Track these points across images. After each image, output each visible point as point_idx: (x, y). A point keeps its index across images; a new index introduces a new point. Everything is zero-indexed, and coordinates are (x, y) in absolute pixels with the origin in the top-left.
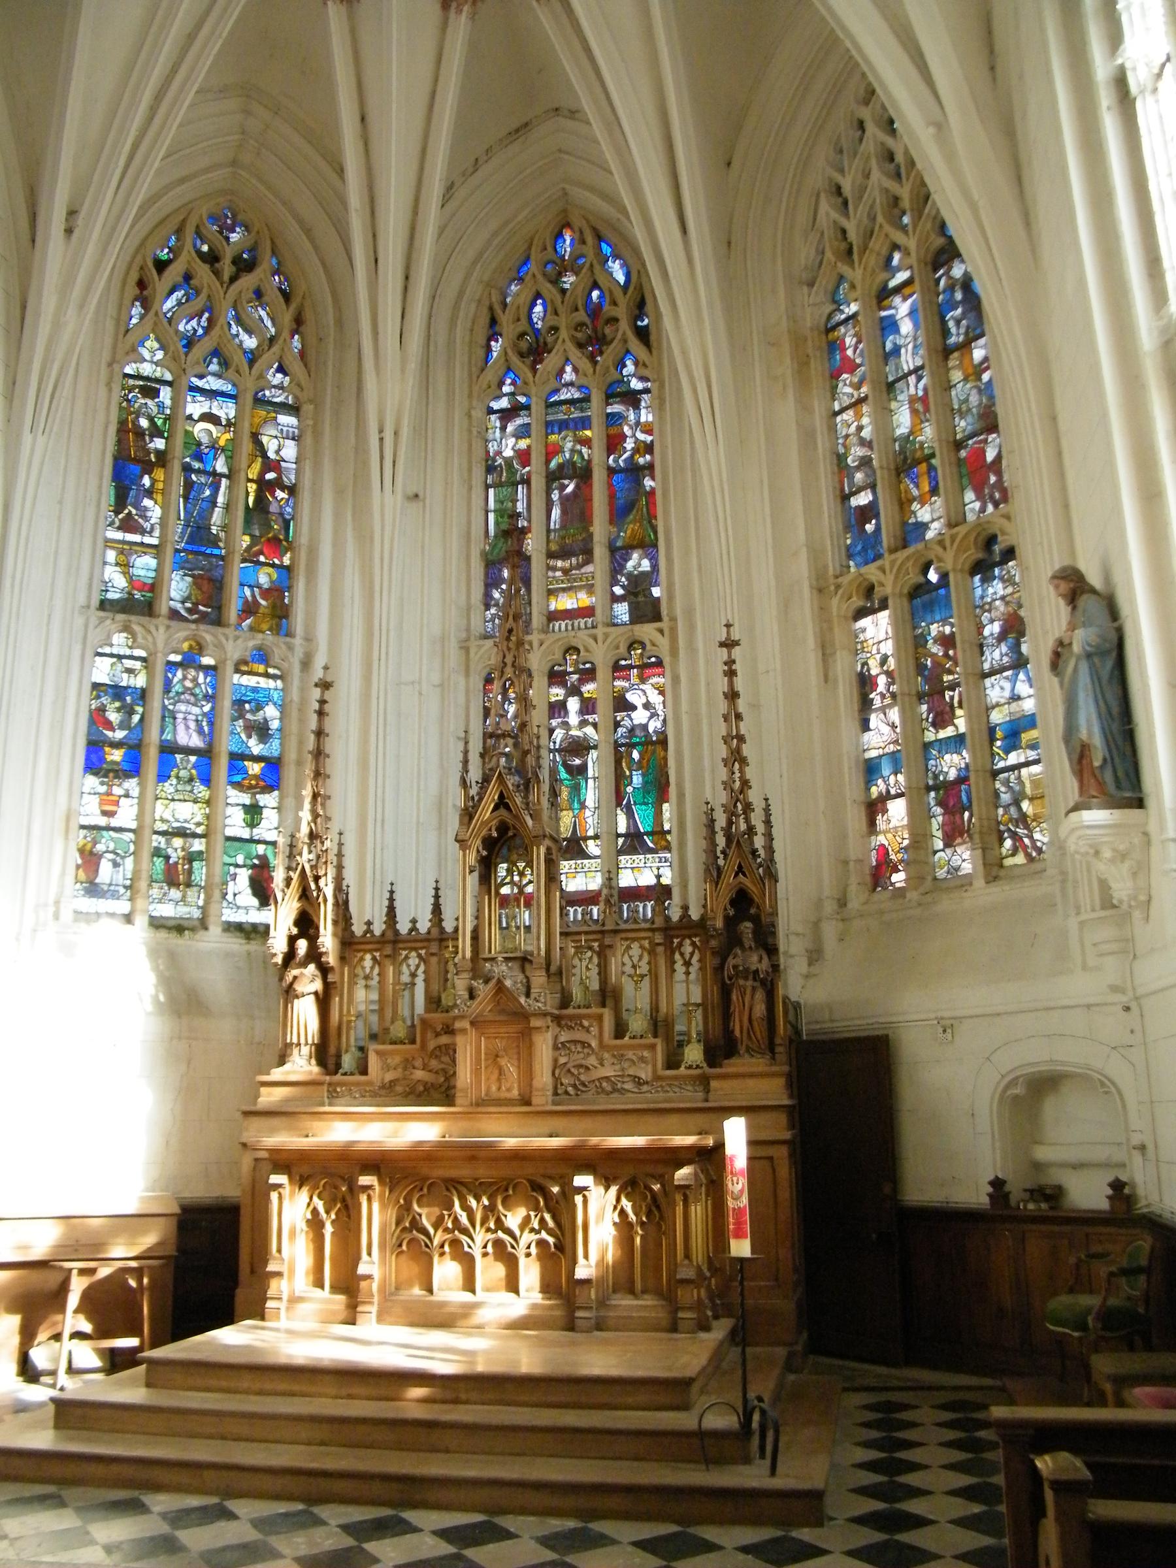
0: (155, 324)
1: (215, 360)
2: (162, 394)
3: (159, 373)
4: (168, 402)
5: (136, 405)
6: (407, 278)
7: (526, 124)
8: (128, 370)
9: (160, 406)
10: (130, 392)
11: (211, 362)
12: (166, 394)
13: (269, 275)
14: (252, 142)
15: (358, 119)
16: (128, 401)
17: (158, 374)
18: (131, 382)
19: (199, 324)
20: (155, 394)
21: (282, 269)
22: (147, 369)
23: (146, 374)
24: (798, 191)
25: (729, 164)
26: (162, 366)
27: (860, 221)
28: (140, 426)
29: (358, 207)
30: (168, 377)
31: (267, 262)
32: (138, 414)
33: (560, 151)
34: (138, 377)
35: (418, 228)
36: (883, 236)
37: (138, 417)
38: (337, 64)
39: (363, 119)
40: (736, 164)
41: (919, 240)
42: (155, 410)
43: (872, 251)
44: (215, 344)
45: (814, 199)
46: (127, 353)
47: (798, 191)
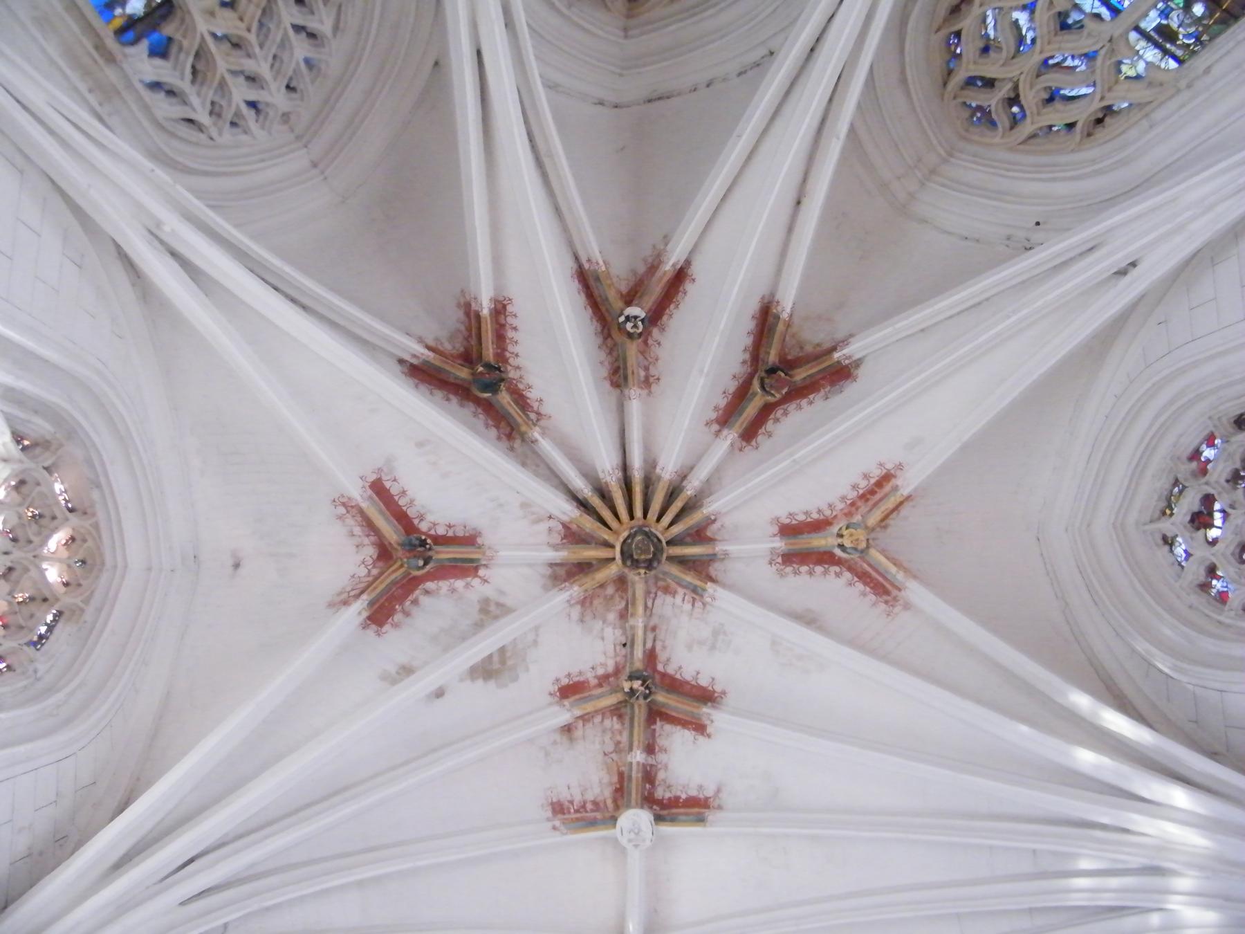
0: (1110, 89)
1: (1070, 21)
2: (1154, 25)
3: (1141, 44)
4: (1153, 14)
5: (1192, 30)
6: (812, 50)
7: (649, 101)
8: (1172, 64)
9: (1165, 14)
10: (1189, 45)
11: (1076, 22)
12: (1151, 22)
13: (964, 59)
14: (919, 174)
15: (803, 206)
16: (1198, 39)
17: (1143, 43)
18: (1179, 53)
19: (1065, 59)
20: (1160, 29)
21: (948, 57)
22: (1151, 54)
23: (1156, 51)
24: (359, 34)
25: (436, 64)
26: (1132, 48)
27: (278, 26)
28: (1207, 8)
29: (834, 140)
30: (1133, 36)
31: (960, 76)
32: (1198, 20)
33: (621, 75)
34: (1166, 52)
35: (782, 94)
36: (246, 19)
37: (1200, 19)
38: (804, 257)
39: (799, 203)
40: (431, 62)
41: (195, 28)
42: (1174, 15)
43: (257, 6)
44: (1059, 38)
45: (342, 25)
46: (1161, 85)
47: (359, 34)
